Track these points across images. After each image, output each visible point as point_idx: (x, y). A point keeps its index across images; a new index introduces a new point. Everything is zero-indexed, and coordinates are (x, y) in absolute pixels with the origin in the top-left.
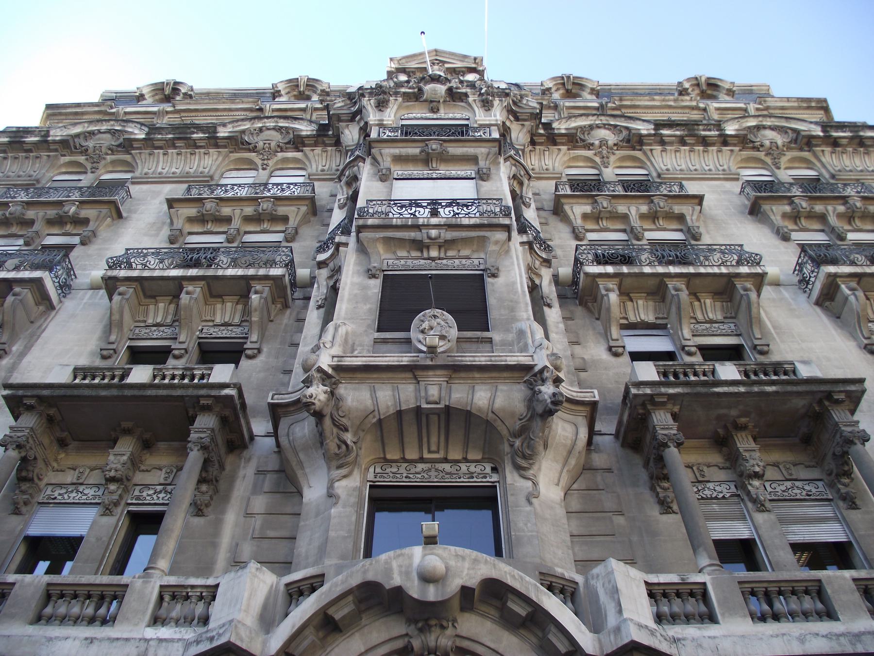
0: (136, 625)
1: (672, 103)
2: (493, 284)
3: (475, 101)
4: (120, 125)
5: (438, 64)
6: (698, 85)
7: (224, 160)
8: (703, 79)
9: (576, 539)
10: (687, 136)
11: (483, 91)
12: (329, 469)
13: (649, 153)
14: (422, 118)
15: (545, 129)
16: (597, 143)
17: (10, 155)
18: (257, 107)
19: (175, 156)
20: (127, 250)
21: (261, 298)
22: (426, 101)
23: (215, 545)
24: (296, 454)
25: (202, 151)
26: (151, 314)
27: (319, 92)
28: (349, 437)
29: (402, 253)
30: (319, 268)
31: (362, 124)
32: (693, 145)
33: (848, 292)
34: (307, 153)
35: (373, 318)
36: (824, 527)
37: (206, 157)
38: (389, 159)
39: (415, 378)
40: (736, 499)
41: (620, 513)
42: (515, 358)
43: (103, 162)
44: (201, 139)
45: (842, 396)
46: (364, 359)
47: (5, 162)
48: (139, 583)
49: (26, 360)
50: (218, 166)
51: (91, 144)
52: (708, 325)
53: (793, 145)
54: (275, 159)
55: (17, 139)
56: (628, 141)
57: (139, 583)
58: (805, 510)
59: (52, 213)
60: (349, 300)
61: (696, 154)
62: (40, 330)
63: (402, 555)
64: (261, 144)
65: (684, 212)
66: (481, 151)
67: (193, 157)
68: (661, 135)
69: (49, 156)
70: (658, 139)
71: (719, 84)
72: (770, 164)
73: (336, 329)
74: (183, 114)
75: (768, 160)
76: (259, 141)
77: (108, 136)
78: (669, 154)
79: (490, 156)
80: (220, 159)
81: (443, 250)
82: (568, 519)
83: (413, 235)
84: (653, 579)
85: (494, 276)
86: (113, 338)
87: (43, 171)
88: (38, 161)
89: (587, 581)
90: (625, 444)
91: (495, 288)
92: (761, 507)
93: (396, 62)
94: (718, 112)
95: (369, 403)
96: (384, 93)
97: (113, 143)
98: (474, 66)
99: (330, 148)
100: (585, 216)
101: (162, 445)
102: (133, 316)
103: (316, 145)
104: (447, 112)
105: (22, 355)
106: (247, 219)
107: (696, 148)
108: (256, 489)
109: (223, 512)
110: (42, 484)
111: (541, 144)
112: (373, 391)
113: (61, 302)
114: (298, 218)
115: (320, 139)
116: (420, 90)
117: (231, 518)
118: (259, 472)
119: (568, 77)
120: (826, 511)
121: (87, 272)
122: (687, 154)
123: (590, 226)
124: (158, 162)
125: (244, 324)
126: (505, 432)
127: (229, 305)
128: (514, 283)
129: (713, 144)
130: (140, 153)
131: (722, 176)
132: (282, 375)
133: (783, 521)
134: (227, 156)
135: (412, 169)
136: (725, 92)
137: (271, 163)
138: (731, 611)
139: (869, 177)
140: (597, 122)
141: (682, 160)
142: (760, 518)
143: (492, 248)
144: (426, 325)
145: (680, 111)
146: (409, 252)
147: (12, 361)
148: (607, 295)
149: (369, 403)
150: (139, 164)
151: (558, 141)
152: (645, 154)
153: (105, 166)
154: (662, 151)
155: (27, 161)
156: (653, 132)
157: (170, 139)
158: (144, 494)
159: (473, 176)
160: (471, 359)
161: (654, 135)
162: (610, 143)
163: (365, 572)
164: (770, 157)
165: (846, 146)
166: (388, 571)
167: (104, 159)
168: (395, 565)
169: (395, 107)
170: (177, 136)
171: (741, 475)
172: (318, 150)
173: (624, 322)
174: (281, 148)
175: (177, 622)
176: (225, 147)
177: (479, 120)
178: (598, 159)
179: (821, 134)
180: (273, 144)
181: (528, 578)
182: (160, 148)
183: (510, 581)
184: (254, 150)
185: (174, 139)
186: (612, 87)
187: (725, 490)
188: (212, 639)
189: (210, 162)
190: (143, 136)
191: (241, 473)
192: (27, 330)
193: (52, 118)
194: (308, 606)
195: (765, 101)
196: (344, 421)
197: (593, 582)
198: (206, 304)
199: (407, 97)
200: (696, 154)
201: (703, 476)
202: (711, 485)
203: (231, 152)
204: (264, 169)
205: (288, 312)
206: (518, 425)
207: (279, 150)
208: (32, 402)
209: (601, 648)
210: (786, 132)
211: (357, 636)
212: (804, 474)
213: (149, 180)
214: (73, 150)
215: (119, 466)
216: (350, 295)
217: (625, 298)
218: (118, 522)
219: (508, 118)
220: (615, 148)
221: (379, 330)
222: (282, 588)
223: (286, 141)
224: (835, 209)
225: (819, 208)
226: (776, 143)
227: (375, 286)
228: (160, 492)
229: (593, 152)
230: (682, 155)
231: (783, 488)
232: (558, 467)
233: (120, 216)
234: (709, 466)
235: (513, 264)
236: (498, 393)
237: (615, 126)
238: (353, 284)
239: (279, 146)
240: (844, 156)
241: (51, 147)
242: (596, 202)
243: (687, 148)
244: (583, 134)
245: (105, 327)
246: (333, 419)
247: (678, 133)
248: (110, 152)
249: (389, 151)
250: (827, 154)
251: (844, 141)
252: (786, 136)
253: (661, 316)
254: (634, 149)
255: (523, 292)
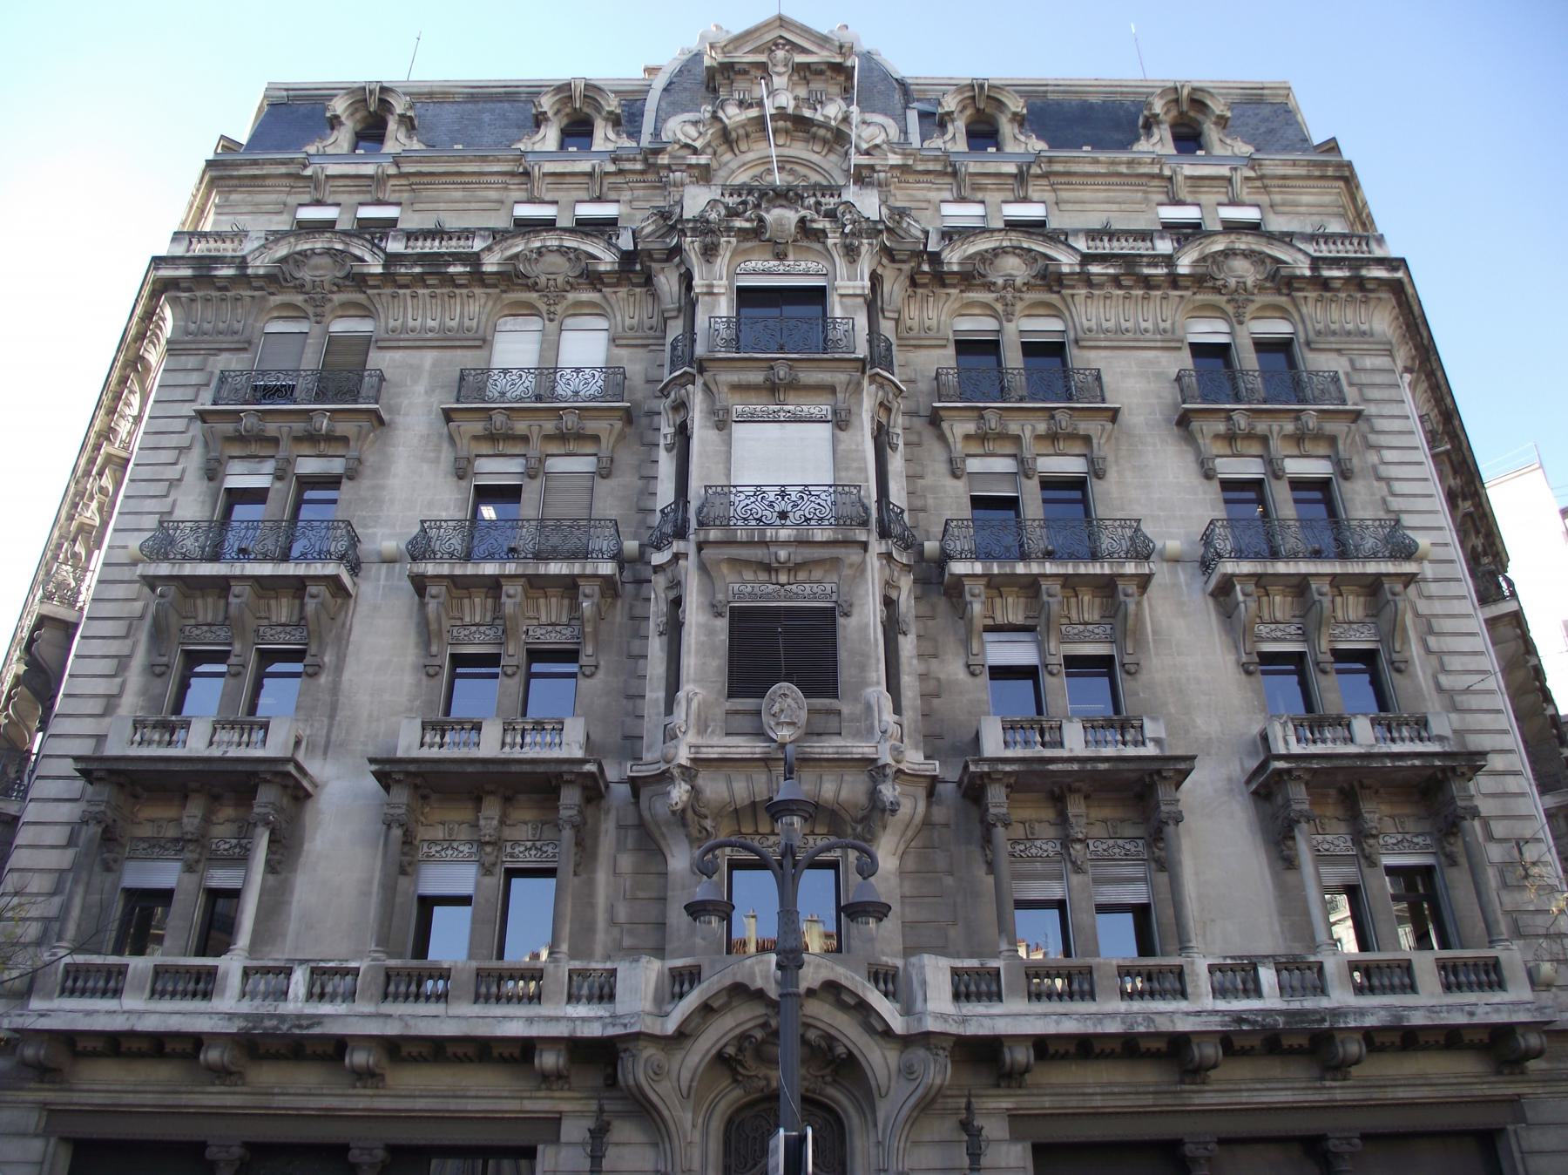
0: (558, 1003)
1: (1123, 169)
2: (845, 627)
3: (835, 244)
4: (343, 242)
5: (784, 45)
6: (1177, 101)
7: (495, 303)
8: (1186, 92)
9: (907, 900)
10: (1123, 275)
11: (847, 230)
12: (691, 847)
13: (1069, 300)
14: (764, 273)
15: (931, 263)
16: (1000, 281)
17: (199, 294)
18: (521, 170)
19: (428, 299)
20: (422, 522)
21: (593, 604)
22: (769, 240)
23: (592, 905)
24: (659, 827)
25: (464, 291)
26: (467, 611)
27: (604, 114)
28: (708, 824)
29: (748, 575)
30: (655, 572)
31: (683, 270)
32: (1130, 288)
33: (1241, 598)
34: (608, 296)
35: (722, 682)
36: (1131, 887)
37: (471, 301)
38: (726, 390)
39: (767, 766)
40: (1059, 858)
41: (951, 873)
42: (860, 750)
43: (329, 306)
44: (460, 274)
45: (1171, 774)
46: (720, 750)
47: (194, 305)
48: (551, 967)
49: (347, 675)
50: (489, 315)
51: (306, 275)
52: (1081, 627)
53: (1268, 285)
54: (565, 304)
55: (204, 273)
56: (1044, 277)
57: (551, 967)
58: (1118, 870)
59: (299, 427)
60: (697, 652)
61: (1133, 301)
62: (346, 632)
63: (762, 961)
64: (543, 280)
65: (1092, 433)
66: (840, 378)
67: (452, 301)
68: (1089, 274)
69: (253, 297)
70: (1085, 277)
71: (1209, 102)
72: (1231, 314)
73: (689, 701)
74: (413, 180)
75: (1230, 309)
76: (538, 271)
77: (326, 260)
78: (1095, 303)
79: (851, 386)
80: (490, 303)
81: (792, 573)
82: (902, 880)
83: (759, 554)
84: (959, 963)
85: (847, 615)
86: (434, 649)
87: (250, 321)
88: (239, 304)
89: (906, 965)
90: (965, 795)
91: (848, 628)
92: (1078, 870)
93: (719, 51)
94: (1189, 182)
95: (726, 795)
96: (712, 232)
97: (338, 274)
98: (838, 60)
99: (638, 290)
100: (967, 437)
101: (522, 797)
102: (448, 614)
103: (617, 285)
104: (798, 258)
105: (339, 669)
106: (548, 438)
107: (1134, 292)
108: (620, 846)
109: (593, 871)
110: (417, 842)
111: (924, 286)
112: (729, 781)
113: (355, 584)
114: (612, 440)
115: (624, 275)
116: (761, 220)
117: (602, 877)
118: (619, 827)
119: (981, 87)
120: (1139, 871)
121: (370, 531)
122: (1121, 301)
123: (975, 448)
124: (405, 308)
125: (573, 622)
126: (848, 818)
127: (554, 600)
128: (867, 625)
129: (1157, 287)
130: (379, 294)
131: (1159, 344)
132: (625, 701)
133: (1097, 881)
134: (499, 298)
135: (754, 401)
136: (1213, 119)
137: (559, 309)
138: (1013, 992)
139: (1356, 346)
140: (1005, 244)
141: (1113, 311)
142: (1076, 879)
143: (847, 572)
144: (776, 708)
145: (1134, 180)
146: (755, 572)
147: (330, 678)
148: (971, 603)
149: (726, 795)
150: (380, 310)
151: (947, 281)
152: (1063, 299)
153: (333, 310)
154: (1087, 297)
155: (224, 304)
156: (1077, 269)
157: (418, 274)
158: (516, 851)
159: (829, 418)
160: (819, 750)
161: (1079, 274)
162: (1019, 282)
163: (734, 975)
164: (1233, 304)
165: (1338, 290)
166: (752, 975)
167: (330, 300)
168: (757, 970)
169: (728, 254)
170: (428, 270)
171: (1067, 836)
172: (623, 291)
173: (989, 622)
174: (572, 286)
175: (590, 1000)
176: (495, 286)
177: (841, 287)
178: (999, 307)
179: (1308, 273)
180: (560, 280)
181: (857, 978)
182: (406, 286)
183: (843, 982)
184: (534, 287)
185: (422, 274)
186: (1049, 88)
187: (1051, 848)
188: (625, 1026)
189: (477, 309)
190: (379, 270)
191: (603, 827)
192: (331, 631)
193: (221, 182)
194: (692, 1000)
195: (1260, 165)
196: (704, 811)
197: (910, 968)
198: (527, 598)
199: (743, 234)
200: (1133, 301)
201: (1032, 834)
202: (1038, 843)
203: (504, 292)
204: (551, 320)
205: (619, 603)
206: (860, 814)
207: (568, 288)
208: (401, 777)
209: (908, 1029)
210: (1263, 262)
211: (729, 1015)
212: (1129, 831)
213: (401, 344)
214: (284, 284)
215: (492, 832)
216: (697, 643)
217: (995, 592)
218: (497, 880)
219: (880, 263)
220: (1025, 289)
221: (731, 695)
222: (667, 971)
223: (577, 273)
224: (1281, 428)
225: (1261, 427)
226: (1245, 283)
227: (722, 624)
228: (530, 849)
229: (994, 295)
230: (1114, 303)
231: (1105, 847)
232: (896, 839)
233: (381, 422)
234: (1040, 822)
235: (867, 590)
236: (844, 785)
237: (1030, 250)
238: (699, 625)
239: (568, 282)
240: (1333, 305)
241: (254, 284)
242: (982, 417)
243: (1121, 292)
244: (984, 263)
245: (418, 624)
246: (695, 812)
247: (1111, 271)
248: (335, 289)
249: (728, 377)
250: (1311, 302)
251: (1337, 284)
252: (1261, 268)
253: (1032, 614)
254: (1051, 291)
255: (876, 640)
